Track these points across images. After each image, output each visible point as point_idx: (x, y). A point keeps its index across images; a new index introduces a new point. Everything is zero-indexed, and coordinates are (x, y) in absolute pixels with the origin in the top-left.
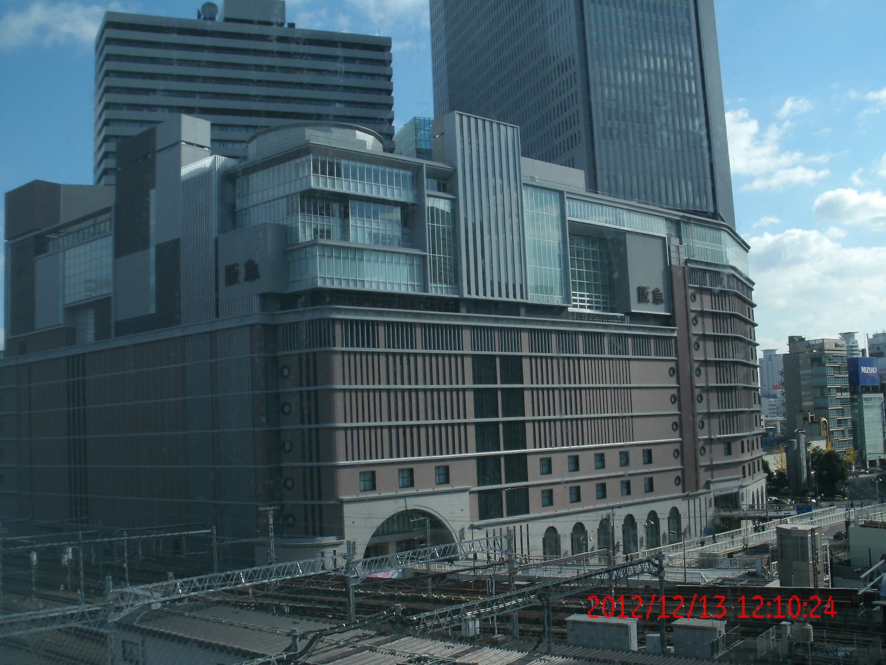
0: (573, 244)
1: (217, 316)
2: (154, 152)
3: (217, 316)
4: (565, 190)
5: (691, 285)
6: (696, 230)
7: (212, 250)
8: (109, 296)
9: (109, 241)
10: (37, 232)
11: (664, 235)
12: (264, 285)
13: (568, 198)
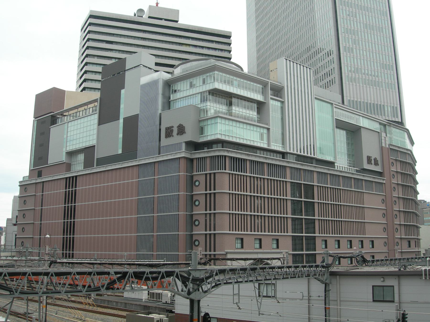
2: (125, 71)
3: (159, 154)
5: (391, 158)
6: (394, 130)
9: (96, 116)
10: (52, 114)
11: (379, 131)
12: (189, 136)
13: (335, 107)
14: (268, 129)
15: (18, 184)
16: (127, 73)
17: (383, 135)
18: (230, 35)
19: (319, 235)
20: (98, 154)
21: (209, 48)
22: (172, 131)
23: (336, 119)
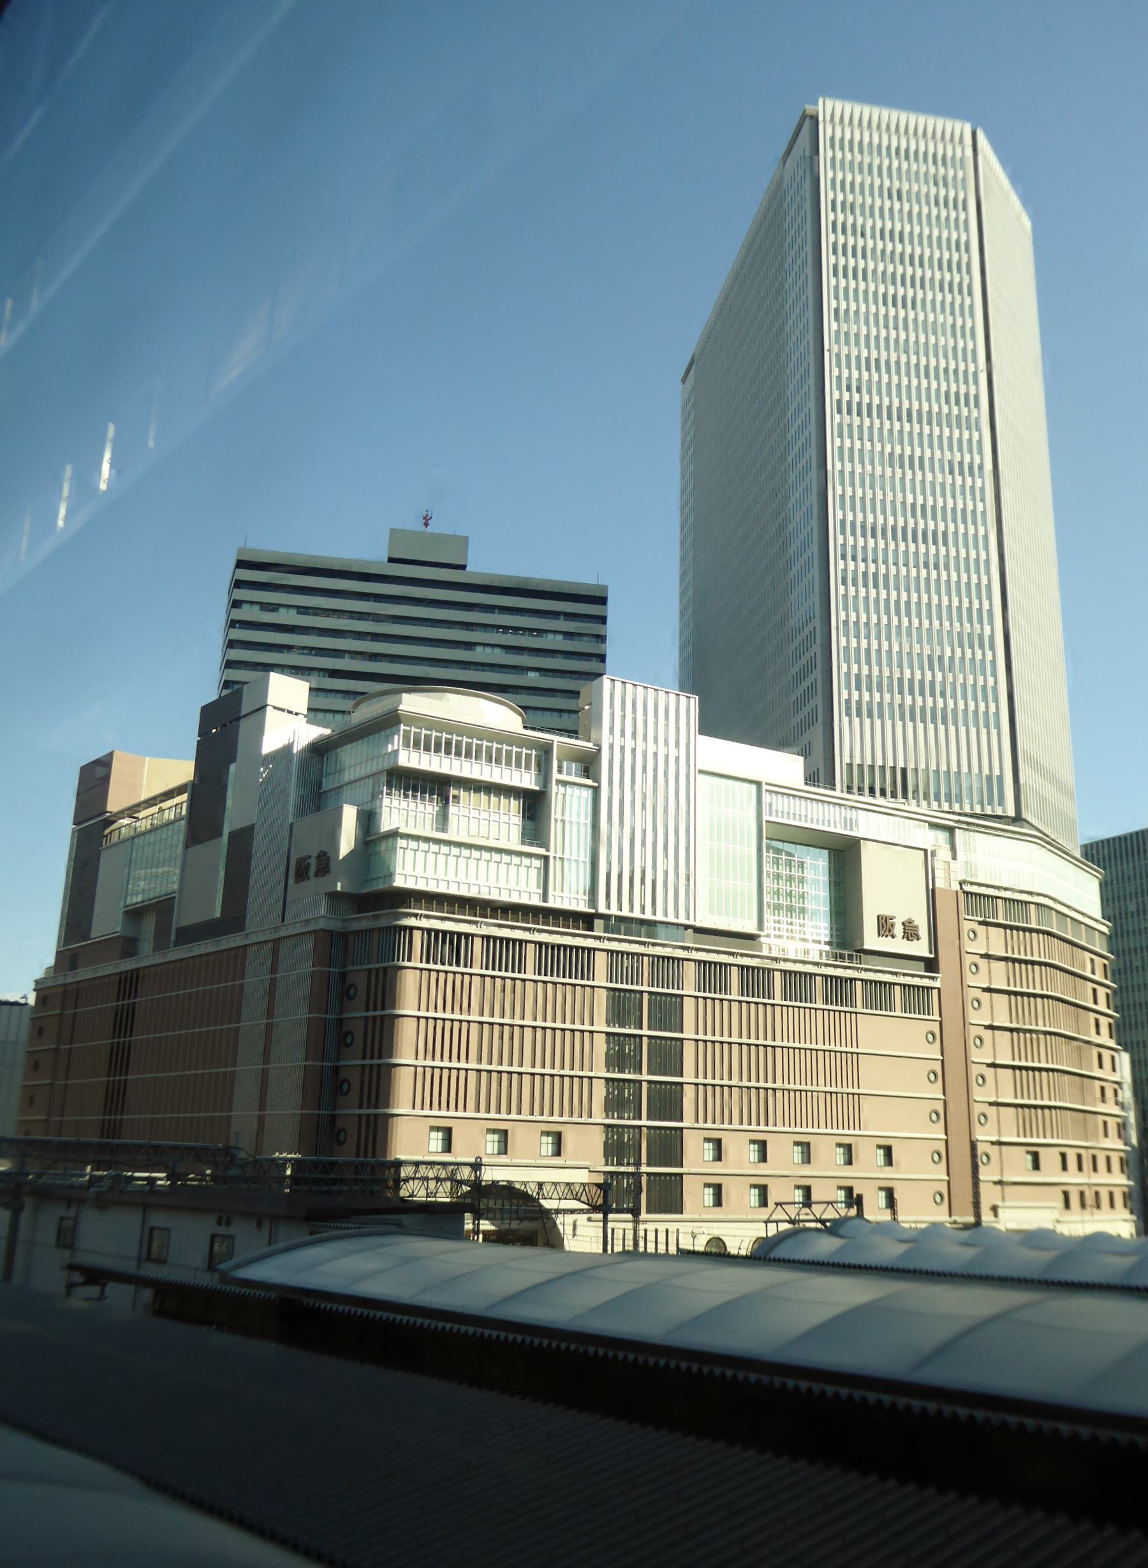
0: (769, 853)
1: (283, 920)
2: (239, 719)
4: (763, 780)
5: (967, 917)
6: (981, 841)
8: (173, 895)
15: (33, 986)
16: (243, 724)
18: (604, 596)
19: (410, 1111)
20: (186, 916)
22: (308, 866)
23: (767, 821)
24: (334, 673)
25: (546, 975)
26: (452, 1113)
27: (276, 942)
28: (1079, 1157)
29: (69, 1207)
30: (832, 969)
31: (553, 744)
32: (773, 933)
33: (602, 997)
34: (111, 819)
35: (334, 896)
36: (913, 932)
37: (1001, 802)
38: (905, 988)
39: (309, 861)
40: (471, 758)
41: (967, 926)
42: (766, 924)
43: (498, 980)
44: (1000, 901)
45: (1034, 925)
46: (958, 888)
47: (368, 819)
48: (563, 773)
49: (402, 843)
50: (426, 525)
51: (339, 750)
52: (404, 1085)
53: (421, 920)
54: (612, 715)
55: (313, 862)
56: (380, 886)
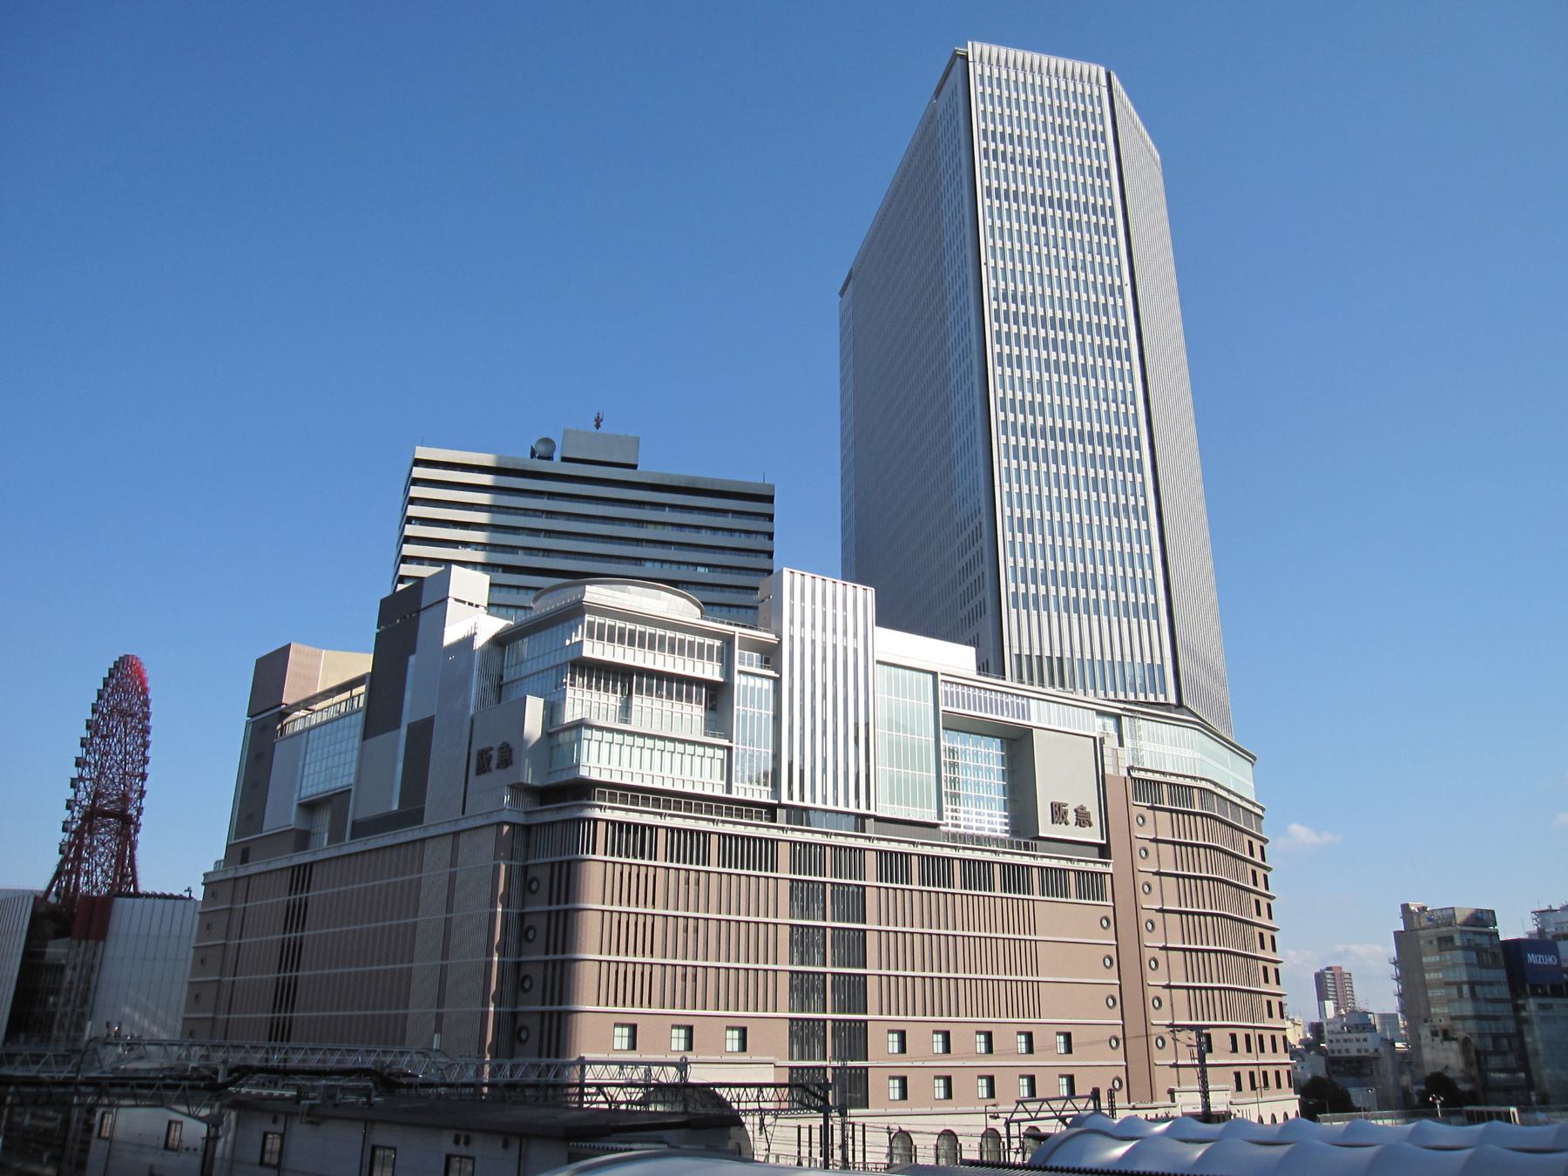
1: (463, 813)
2: (418, 612)
5: (1136, 803)
6: (1145, 726)
7: (467, 729)
8: (349, 788)
14: (730, 749)
15: (202, 879)
16: (423, 616)
17: (1111, 742)
20: (358, 811)
21: (715, 529)
22: (489, 759)
23: (943, 711)
24: (508, 569)
25: (730, 867)
26: (637, 1009)
27: (456, 834)
28: (1248, 1037)
29: (275, 1120)
30: (939, 848)
31: (734, 636)
32: (950, 821)
33: (784, 887)
34: (287, 711)
35: (518, 789)
36: (1085, 819)
37: (1164, 692)
38: (1079, 874)
39: (491, 753)
40: (634, 646)
41: (1135, 811)
42: (945, 813)
43: (762, 880)
44: (1195, 790)
45: (1197, 810)
46: (1126, 774)
47: (552, 710)
48: (745, 661)
49: (586, 733)
50: (598, 426)
51: (520, 642)
52: (587, 980)
53: (606, 812)
54: (792, 606)
55: (495, 754)
56: (565, 777)
